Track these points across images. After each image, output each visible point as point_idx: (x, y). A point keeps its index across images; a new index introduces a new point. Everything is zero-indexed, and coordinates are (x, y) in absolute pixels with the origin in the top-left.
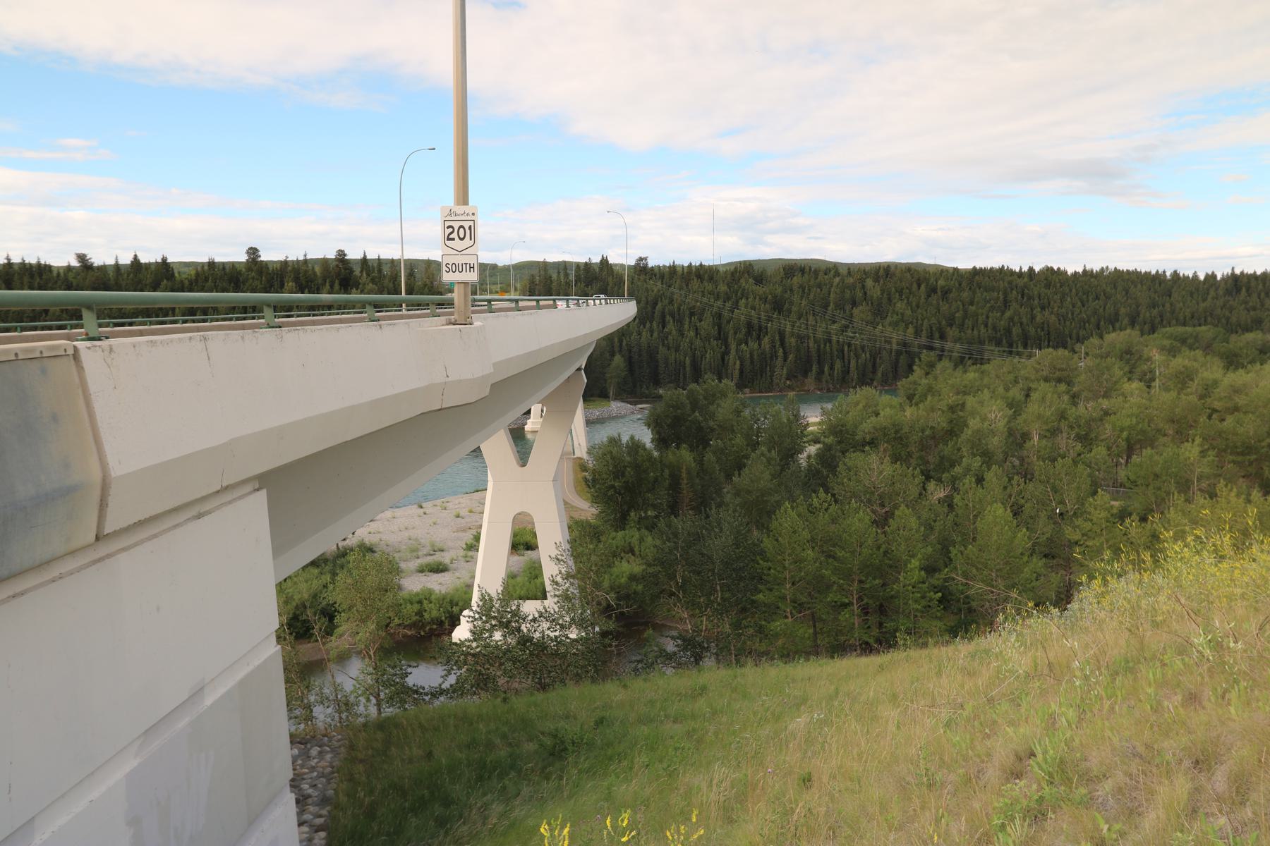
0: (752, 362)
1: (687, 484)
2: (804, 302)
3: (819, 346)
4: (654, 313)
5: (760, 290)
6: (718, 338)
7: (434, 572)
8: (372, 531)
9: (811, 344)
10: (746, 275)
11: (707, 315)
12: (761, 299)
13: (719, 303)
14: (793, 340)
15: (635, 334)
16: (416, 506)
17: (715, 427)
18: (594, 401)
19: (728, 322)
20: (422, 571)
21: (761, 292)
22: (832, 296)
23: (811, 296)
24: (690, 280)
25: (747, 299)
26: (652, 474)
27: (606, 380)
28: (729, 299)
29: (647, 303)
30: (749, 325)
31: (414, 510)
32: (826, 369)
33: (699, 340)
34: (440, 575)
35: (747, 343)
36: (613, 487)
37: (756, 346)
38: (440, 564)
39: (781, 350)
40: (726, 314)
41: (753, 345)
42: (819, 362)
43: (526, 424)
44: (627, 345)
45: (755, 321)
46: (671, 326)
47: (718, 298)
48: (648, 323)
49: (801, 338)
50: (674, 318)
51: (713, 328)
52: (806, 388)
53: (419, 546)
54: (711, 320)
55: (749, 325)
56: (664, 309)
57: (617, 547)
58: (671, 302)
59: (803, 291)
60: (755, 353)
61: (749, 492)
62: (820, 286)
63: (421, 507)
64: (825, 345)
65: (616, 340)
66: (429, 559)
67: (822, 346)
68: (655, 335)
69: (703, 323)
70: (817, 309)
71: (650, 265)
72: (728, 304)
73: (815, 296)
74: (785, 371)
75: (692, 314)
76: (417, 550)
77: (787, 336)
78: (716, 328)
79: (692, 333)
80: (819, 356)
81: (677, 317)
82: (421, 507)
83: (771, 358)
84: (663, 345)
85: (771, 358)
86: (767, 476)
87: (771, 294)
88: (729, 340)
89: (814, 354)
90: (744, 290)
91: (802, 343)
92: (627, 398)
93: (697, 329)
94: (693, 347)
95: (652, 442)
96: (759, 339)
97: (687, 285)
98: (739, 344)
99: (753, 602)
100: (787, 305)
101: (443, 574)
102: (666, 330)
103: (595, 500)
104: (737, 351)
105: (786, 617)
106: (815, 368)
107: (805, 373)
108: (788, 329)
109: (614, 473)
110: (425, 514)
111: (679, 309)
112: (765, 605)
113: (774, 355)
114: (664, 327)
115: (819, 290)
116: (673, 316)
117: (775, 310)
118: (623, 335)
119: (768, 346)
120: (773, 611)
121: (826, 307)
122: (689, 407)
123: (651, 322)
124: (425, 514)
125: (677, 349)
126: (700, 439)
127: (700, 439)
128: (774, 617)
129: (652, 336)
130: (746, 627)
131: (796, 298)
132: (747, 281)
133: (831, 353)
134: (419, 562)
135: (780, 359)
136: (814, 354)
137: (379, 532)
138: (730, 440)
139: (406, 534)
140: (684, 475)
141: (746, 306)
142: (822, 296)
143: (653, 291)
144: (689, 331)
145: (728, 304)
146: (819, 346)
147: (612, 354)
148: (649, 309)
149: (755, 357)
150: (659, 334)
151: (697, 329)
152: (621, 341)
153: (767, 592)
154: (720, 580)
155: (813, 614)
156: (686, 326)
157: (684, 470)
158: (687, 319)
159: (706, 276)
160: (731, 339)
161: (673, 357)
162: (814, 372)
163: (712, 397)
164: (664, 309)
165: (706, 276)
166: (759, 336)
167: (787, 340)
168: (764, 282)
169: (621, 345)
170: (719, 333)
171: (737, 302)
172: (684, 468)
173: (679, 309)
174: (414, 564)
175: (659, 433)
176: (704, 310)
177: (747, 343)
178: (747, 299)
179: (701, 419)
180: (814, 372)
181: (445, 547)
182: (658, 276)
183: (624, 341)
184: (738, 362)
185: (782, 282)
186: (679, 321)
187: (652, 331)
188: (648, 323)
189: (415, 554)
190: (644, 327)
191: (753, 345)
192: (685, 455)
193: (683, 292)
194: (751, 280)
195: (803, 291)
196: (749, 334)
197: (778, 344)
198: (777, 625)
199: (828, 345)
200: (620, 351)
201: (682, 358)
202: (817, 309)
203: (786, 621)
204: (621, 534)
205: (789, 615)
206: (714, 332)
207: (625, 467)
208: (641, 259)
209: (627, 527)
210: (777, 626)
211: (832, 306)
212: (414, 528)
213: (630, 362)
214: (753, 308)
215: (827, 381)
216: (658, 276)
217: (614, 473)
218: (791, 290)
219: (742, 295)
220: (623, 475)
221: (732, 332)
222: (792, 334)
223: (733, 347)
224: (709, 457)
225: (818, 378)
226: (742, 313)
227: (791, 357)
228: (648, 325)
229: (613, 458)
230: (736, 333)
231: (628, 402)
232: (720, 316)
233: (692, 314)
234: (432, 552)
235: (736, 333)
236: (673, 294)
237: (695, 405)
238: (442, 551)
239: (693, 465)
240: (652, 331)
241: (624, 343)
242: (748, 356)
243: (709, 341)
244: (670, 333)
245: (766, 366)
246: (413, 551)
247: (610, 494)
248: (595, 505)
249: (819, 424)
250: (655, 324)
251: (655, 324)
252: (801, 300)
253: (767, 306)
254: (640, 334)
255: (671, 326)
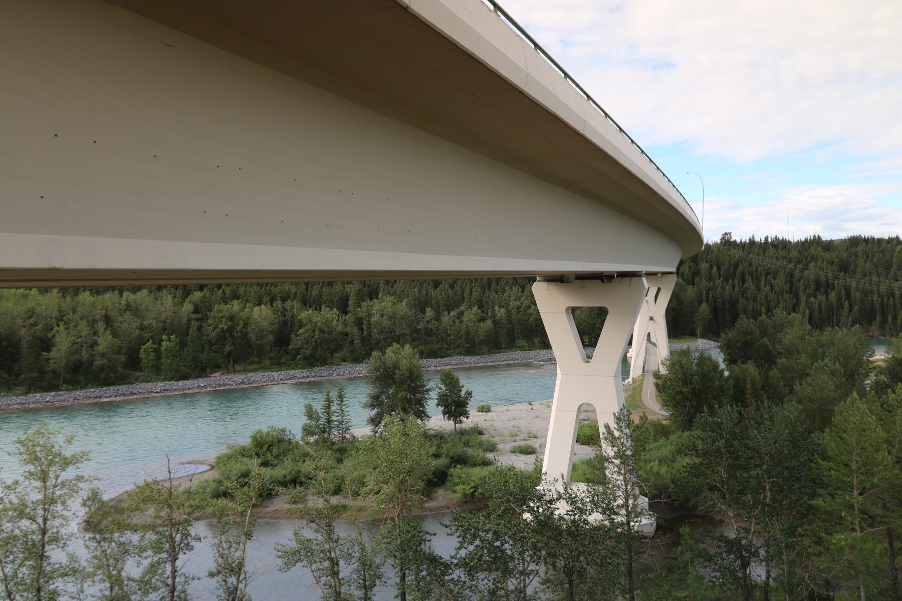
0: (820, 312)
1: (752, 394)
2: (868, 265)
3: (882, 300)
4: (736, 273)
5: (827, 255)
6: (790, 292)
7: (524, 453)
8: (487, 419)
9: (875, 298)
10: (815, 245)
11: (781, 275)
12: (828, 262)
13: (791, 265)
14: (858, 295)
15: (719, 288)
16: (527, 403)
17: (782, 350)
18: (685, 338)
19: (799, 280)
20: (514, 452)
21: (828, 257)
22: (894, 260)
23: (875, 260)
24: (766, 249)
25: (816, 262)
26: (717, 383)
27: (694, 322)
28: (799, 262)
29: (730, 266)
30: (818, 282)
31: (526, 406)
32: (890, 318)
33: (773, 294)
34: (528, 456)
35: (815, 297)
36: (681, 392)
37: (824, 299)
38: (530, 447)
39: (847, 302)
40: (797, 274)
41: (821, 298)
42: (883, 313)
43: (628, 352)
44: (712, 297)
45: (823, 279)
46: (749, 283)
47: (790, 261)
48: (731, 280)
49: (865, 293)
50: (752, 276)
51: (786, 284)
52: (871, 334)
53: (519, 433)
54: (784, 278)
55: (818, 282)
56: (744, 270)
57: (682, 445)
58: (750, 264)
59: (867, 257)
60: (823, 304)
61: (812, 401)
62: (882, 252)
63: (531, 404)
64: (889, 299)
65: (704, 293)
66: (522, 443)
67: (886, 300)
68: (737, 289)
69: (777, 280)
70: (881, 270)
71: (733, 239)
72: (800, 266)
73: (878, 259)
74: (850, 319)
75: (767, 274)
76: (517, 435)
77: (853, 291)
78: (788, 284)
79: (768, 288)
80: (882, 308)
81: (755, 276)
82: (531, 404)
83: (838, 309)
84: (743, 297)
85: (838, 309)
86: (831, 386)
87: (838, 258)
88: (800, 294)
89: (878, 306)
90: (813, 255)
91: (867, 297)
92: (712, 337)
93: (772, 286)
94: (768, 299)
95: (724, 361)
96: (826, 293)
97: (764, 253)
98: (809, 296)
99: (810, 507)
100: (852, 267)
101: (531, 456)
102: (745, 286)
103: (665, 404)
104: (807, 302)
105: (854, 530)
106: (878, 317)
107: (870, 322)
108: (854, 284)
109: (682, 380)
110: (532, 409)
111: (757, 270)
112: (827, 512)
113: (840, 306)
114: (743, 283)
115: (881, 255)
116: (751, 275)
117: (841, 271)
118: (710, 289)
119: (835, 299)
120: (835, 522)
121: (889, 268)
122: (758, 333)
123: (733, 280)
124: (532, 409)
125: (755, 300)
126: (767, 359)
127: (767, 359)
128: (838, 527)
129: (733, 290)
130: (802, 536)
131: (861, 261)
132: (816, 249)
133: (895, 306)
134: (516, 444)
135: (846, 310)
136: (878, 306)
137: (492, 420)
138: (796, 359)
139: (512, 423)
140: (749, 386)
141: (815, 267)
142: (885, 259)
143: (735, 257)
144: (765, 286)
145: (800, 266)
146: (882, 300)
147: (700, 303)
148: (732, 270)
149: (823, 307)
150: (739, 289)
151: (772, 286)
152: (708, 294)
153: (829, 498)
154: (769, 478)
155: (889, 529)
156: (763, 283)
157: (748, 382)
158: (763, 278)
159: (780, 245)
160: (801, 294)
161: (751, 306)
162: (878, 321)
163: (780, 327)
164: (744, 270)
165: (780, 245)
166: (827, 291)
167: (852, 294)
168: (831, 250)
169: (708, 297)
170: (791, 288)
171: (807, 265)
172: (749, 379)
173: (757, 270)
174: (508, 447)
175: (730, 354)
176: (778, 271)
177: (815, 297)
178: (816, 262)
179: (769, 343)
180: (878, 321)
181: (539, 435)
182: (740, 246)
183: (711, 293)
184: (807, 311)
185: (847, 250)
186: (757, 279)
187: (734, 287)
188: (731, 280)
189: (514, 438)
190: (727, 283)
191: (821, 298)
192: (751, 369)
193: (760, 258)
194: (819, 248)
195: (867, 257)
196: (817, 289)
197: (844, 297)
198: (840, 538)
199: (891, 298)
200: (707, 302)
201: (759, 308)
202: (881, 270)
203: (854, 534)
204: (687, 433)
205: (857, 528)
206: (787, 287)
207: (692, 375)
208: (726, 234)
209: (693, 428)
210: (840, 540)
211: (894, 267)
212: (520, 419)
213: (715, 310)
214: (822, 269)
215: (890, 329)
216: (740, 246)
217: (682, 380)
218: (856, 256)
219: (812, 259)
220: (691, 383)
221: (802, 288)
222: (857, 290)
223: (803, 299)
224: (774, 372)
225: (882, 325)
226: (811, 272)
227: (856, 308)
228: (730, 282)
229: (682, 367)
230: (805, 289)
231: (712, 340)
232: (791, 275)
233: (767, 274)
234: (527, 438)
235: (805, 289)
236: (751, 259)
237: (764, 333)
238: (536, 438)
239: (758, 378)
240: (734, 287)
241: (710, 296)
242: (817, 307)
243: (782, 295)
244: (748, 288)
245: (833, 316)
246: (512, 436)
247: (678, 398)
248: (665, 408)
249: (884, 361)
250: (736, 281)
251: (736, 281)
252: (866, 263)
253: (834, 267)
254: (723, 288)
255: (749, 283)
